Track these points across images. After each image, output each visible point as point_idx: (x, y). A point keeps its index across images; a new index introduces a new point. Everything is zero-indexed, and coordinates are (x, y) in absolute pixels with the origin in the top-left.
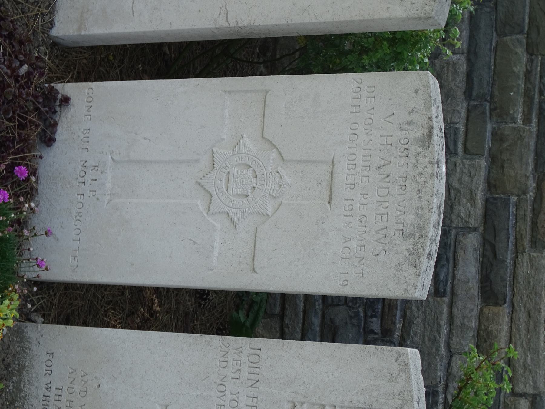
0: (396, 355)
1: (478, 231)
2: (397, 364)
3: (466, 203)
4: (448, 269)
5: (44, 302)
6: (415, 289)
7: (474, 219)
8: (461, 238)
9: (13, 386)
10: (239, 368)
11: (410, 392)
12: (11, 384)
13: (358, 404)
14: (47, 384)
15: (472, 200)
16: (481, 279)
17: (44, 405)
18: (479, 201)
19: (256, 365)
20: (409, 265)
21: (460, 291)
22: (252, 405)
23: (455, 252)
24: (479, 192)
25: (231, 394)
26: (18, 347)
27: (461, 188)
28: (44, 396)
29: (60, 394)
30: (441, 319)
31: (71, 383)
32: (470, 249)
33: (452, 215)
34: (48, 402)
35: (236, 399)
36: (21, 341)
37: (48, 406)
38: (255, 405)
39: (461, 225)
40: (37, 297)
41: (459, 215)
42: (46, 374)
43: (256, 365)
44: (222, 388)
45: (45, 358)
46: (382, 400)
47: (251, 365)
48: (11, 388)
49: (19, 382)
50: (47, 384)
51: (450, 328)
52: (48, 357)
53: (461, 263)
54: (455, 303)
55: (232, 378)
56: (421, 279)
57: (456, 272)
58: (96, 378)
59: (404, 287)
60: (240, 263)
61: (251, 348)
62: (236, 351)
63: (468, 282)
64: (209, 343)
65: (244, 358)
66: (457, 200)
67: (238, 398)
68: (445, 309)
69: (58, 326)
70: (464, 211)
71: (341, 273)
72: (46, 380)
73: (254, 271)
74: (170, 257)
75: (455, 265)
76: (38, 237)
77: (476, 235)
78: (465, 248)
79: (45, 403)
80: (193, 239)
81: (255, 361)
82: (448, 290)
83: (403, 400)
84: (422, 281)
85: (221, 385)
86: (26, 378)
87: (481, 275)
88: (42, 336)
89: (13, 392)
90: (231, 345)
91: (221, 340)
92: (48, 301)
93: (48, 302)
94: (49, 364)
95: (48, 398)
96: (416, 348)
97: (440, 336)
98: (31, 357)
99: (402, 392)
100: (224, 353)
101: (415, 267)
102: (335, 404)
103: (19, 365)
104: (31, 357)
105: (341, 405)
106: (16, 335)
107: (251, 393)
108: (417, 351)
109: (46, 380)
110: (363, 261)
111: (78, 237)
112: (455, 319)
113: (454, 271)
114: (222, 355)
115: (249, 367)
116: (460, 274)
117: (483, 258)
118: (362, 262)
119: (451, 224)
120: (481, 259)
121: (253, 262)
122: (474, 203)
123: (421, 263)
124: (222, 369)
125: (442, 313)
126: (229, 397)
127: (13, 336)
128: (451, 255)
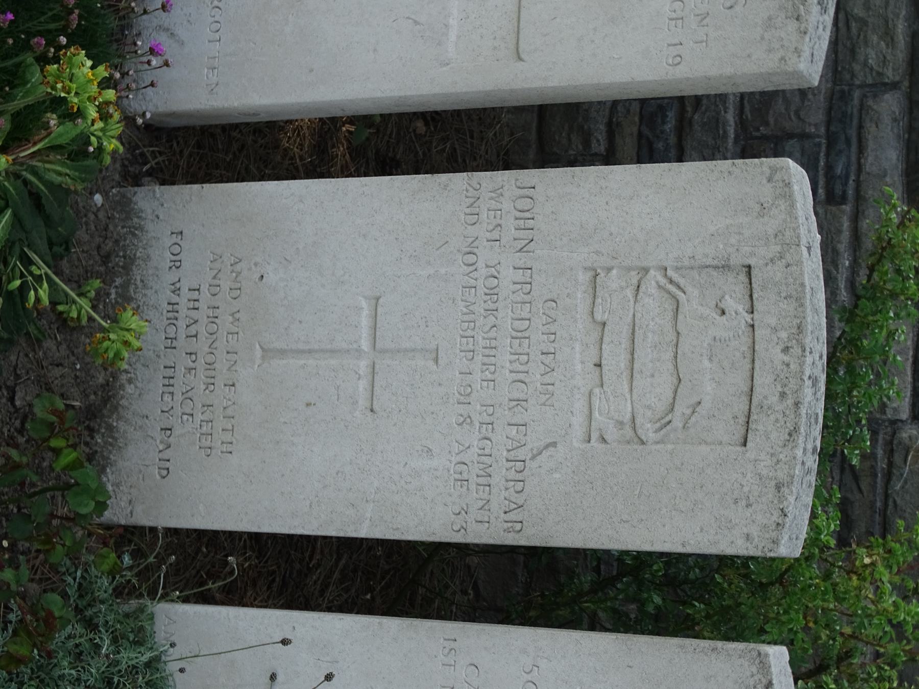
0: (768, 171)
1: (900, 89)
2: (769, 185)
3: (878, 43)
4: (849, 157)
5: (164, 161)
6: (799, 56)
7: (893, 69)
8: (870, 102)
9: (117, 293)
10: (499, 222)
11: (794, 230)
12: (113, 291)
13: (704, 260)
14: (173, 284)
15: (888, 35)
16: (907, 169)
17: (170, 319)
18: (901, 37)
19: (527, 215)
20: (786, 18)
21: (870, 192)
22: (523, 280)
23: (860, 127)
24: (901, 21)
25: (487, 266)
26: (123, 227)
27: (869, 16)
28: (169, 304)
29: (195, 297)
30: (839, 242)
31: (214, 278)
32: (887, 120)
33: (854, 65)
34: (176, 314)
35: (496, 274)
36: (128, 218)
37: (177, 319)
38: (529, 280)
39: (870, 81)
40: (151, 149)
41: (865, 64)
42: (170, 268)
43: (527, 215)
44: (471, 259)
45: (168, 241)
46: (747, 249)
47: (519, 214)
48: (113, 296)
49: (125, 286)
50: (173, 284)
51: (855, 256)
52: (175, 238)
53: (871, 144)
54: (863, 213)
55: (488, 241)
56: (807, 39)
57: (862, 161)
58: (256, 264)
59: (779, 55)
60: (495, 48)
61: (519, 188)
62: (493, 195)
63: (885, 176)
64: (446, 186)
65: (506, 205)
66: (862, 37)
67: (498, 273)
68: (846, 224)
69: (189, 186)
70: (874, 56)
71: (669, 45)
72: (172, 277)
73: (520, 59)
74: (375, 50)
75: (861, 149)
76: (150, 16)
77: (896, 96)
78: (878, 118)
79: (170, 315)
80: (413, 17)
81: (526, 208)
82: (850, 192)
83: (782, 245)
84: (811, 45)
85: (470, 253)
86: (138, 278)
87: (907, 163)
88: (162, 205)
89: (117, 302)
90: (484, 185)
91: (466, 178)
92: (170, 161)
93: (170, 164)
94: (176, 249)
95: (175, 306)
96: (782, 643)
97: (837, 270)
98: (145, 242)
99: (780, 231)
100: (472, 200)
101: (797, 19)
102: (665, 264)
103: (124, 257)
104: (145, 242)
105: (675, 264)
106: (119, 208)
107: (522, 261)
108: (784, 648)
109: (172, 277)
110: (707, 20)
111: (217, 36)
112: (864, 240)
113: (859, 159)
114: (468, 204)
115: (517, 219)
116: (870, 163)
117: (910, 133)
118: (705, 22)
119: (852, 79)
120: (906, 136)
121: (517, 43)
122: (892, 39)
123: (808, 12)
124: (469, 227)
125: (840, 232)
126: (483, 271)
127: (114, 210)
128: (853, 133)
